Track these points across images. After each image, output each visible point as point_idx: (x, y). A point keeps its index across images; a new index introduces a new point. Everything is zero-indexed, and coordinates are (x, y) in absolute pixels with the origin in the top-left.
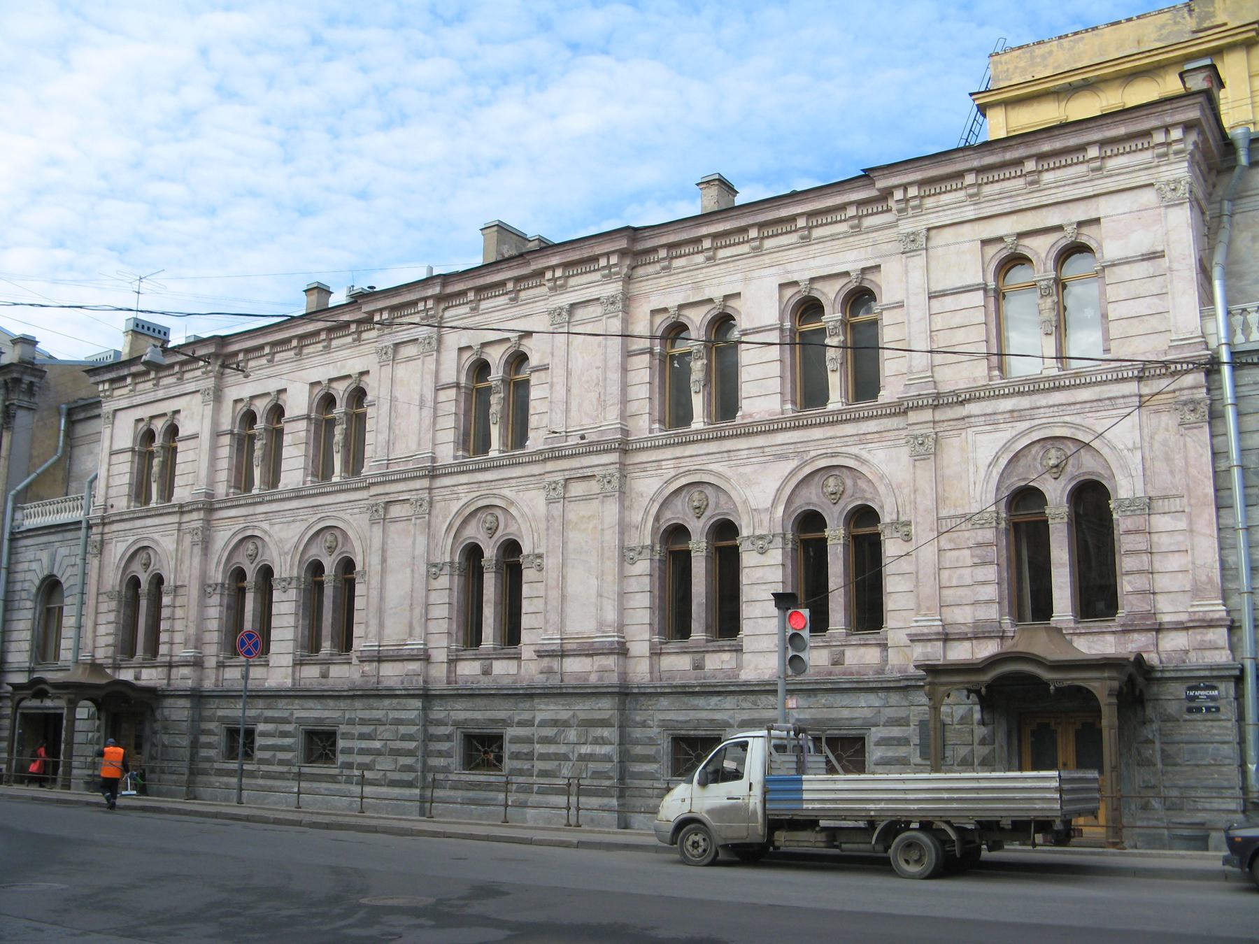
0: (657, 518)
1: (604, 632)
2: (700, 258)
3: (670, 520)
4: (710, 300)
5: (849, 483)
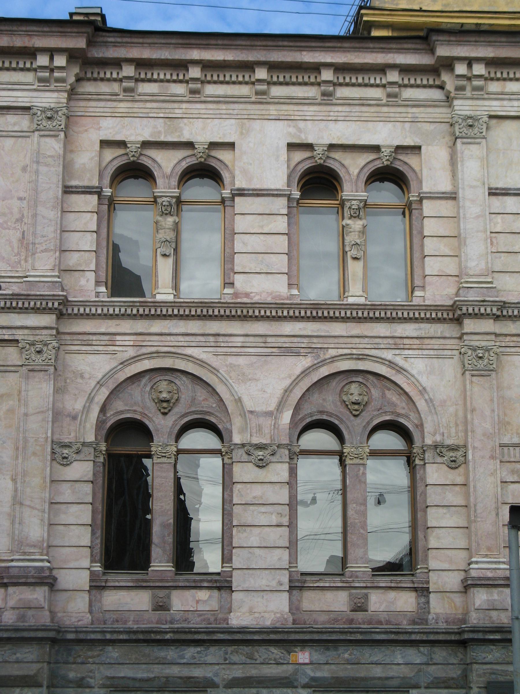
0: (103, 409)
1: (24, 553)
2: (180, 89)
3: (122, 412)
4: (190, 145)
5: (375, 393)
